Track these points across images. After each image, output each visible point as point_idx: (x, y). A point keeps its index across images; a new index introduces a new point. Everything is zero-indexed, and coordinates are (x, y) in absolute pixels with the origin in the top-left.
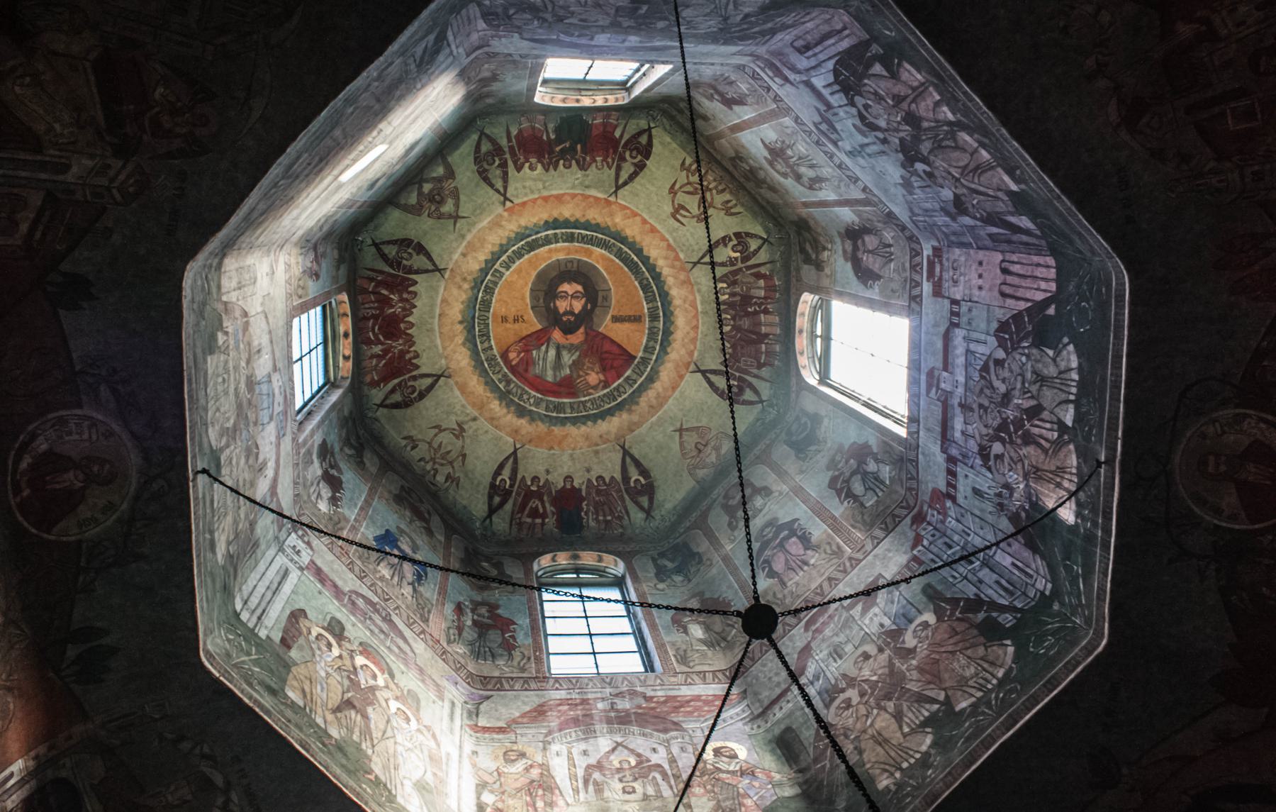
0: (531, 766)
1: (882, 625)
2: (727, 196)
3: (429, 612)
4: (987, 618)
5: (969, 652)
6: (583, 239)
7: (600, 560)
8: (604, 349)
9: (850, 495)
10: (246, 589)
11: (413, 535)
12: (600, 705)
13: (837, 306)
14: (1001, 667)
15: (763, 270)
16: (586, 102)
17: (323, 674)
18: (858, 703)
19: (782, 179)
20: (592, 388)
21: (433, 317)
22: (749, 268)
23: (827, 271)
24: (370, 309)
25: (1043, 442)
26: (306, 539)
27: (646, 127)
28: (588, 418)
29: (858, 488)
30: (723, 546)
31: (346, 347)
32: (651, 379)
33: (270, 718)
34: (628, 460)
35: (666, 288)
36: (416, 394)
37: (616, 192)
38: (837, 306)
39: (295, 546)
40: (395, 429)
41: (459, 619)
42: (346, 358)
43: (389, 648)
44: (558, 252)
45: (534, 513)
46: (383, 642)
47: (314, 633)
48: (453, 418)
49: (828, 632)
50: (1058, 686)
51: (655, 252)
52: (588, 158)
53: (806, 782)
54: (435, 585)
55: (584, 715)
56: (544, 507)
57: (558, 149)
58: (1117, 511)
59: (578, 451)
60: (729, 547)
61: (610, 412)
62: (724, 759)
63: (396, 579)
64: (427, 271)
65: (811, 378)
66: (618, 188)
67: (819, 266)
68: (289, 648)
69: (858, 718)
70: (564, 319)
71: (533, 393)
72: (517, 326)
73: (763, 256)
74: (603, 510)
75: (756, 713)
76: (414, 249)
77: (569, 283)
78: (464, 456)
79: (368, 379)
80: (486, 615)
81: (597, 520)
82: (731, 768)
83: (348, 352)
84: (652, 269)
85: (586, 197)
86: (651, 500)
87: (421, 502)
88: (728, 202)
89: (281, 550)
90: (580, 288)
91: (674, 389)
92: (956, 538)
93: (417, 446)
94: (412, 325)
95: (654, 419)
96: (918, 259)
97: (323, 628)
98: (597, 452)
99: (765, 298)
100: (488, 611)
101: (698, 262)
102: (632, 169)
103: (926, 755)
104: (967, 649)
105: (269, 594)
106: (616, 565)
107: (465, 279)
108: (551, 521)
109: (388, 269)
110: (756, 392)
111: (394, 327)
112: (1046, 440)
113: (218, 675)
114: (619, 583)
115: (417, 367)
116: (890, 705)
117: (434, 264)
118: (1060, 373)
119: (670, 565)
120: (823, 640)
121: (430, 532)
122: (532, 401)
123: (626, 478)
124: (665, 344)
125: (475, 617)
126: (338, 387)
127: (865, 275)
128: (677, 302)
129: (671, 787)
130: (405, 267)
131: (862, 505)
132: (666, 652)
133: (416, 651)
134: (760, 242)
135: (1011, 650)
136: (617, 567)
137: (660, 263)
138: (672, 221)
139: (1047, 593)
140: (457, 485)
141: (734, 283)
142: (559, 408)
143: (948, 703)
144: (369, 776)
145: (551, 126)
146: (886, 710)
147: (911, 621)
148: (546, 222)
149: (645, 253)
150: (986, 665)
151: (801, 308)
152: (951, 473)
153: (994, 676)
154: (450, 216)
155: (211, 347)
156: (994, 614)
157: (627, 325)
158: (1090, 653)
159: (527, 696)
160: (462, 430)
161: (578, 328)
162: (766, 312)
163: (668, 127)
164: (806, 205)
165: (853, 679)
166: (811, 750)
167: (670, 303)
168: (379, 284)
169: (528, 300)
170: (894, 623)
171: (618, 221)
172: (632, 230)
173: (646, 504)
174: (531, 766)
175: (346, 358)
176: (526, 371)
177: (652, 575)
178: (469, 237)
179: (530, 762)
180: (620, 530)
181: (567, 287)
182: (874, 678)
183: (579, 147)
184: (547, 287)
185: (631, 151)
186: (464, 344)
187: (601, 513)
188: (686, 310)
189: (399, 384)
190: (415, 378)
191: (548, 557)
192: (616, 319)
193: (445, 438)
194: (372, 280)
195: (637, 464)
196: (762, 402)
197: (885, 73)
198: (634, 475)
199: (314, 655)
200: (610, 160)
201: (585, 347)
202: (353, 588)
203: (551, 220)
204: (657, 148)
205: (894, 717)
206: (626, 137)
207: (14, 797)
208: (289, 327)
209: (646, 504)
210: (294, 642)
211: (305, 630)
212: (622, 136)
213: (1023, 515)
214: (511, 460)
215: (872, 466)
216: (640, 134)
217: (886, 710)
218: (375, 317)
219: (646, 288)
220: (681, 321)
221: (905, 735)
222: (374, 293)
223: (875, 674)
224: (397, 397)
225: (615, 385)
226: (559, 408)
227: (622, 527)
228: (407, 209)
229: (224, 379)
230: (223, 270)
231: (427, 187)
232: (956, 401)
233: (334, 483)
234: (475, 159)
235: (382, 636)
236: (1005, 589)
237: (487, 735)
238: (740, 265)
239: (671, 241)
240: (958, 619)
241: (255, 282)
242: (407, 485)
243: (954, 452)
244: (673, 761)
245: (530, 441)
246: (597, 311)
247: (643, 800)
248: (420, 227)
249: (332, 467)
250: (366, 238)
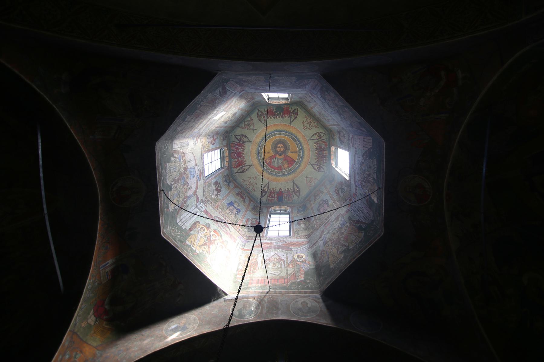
0: (253, 259)
1: (339, 226)
2: (315, 124)
3: (238, 221)
4: (360, 225)
5: (354, 234)
6: (283, 134)
7: (286, 208)
8: (288, 159)
9: (338, 194)
10: (182, 217)
11: (239, 203)
12: (274, 244)
13: (339, 149)
14: (360, 238)
15: (324, 141)
16: (281, 103)
17: (200, 237)
18: (331, 245)
19: (322, 119)
20: (286, 168)
21: (249, 152)
22: (321, 140)
23: (335, 141)
24: (233, 150)
25: (371, 182)
26: (205, 204)
27: (296, 108)
28: (285, 175)
29: (340, 192)
30: (312, 205)
31: (227, 159)
32: (299, 166)
33: (178, 248)
34: (294, 185)
35: (302, 145)
36: (245, 170)
37: (290, 123)
38: (339, 149)
39: (201, 206)
40: (240, 178)
41: (247, 222)
42: (227, 162)
43: (223, 230)
44: (278, 137)
45: (272, 197)
46: (221, 229)
47: (200, 227)
48: (254, 175)
49: (328, 227)
50: (371, 244)
51: (300, 137)
52: (284, 116)
53: (317, 265)
54: (242, 214)
55: (270, 246)
56: (275, 195)
57: (276, 114)
58: (384, 201)
59: (283, 183)
60: (313, 205)
61: (290, 174)
62: (300, 258)
63: (230, 213)
64: (247, 142)
65: (334, 166)
66: (291, 122)
67: (334, 140)
68: (191, 231)
69: (330, 249)
70: (279, 152)
71: (272, 169)
72: (268, 154)
73: (324, 138)
74: (288, 196)
75: (311, 246)
76: (244, 137)
77: (280, 144)
78: (256, 184)
79: (233, 166)
80: (255, 221)
81: (287, 198)
82: (300, 261)
83: (227, 160)
84: (299, 141)
85: (283, 125)
86: (299, 194)
87: (244, 195)
88: (316, 125)
89: (197, 207)
90: (282, 145)
91: (305, 168)
92: (357, 205)
93: (245, 182)
94: (244, 154)
95: (300, 175)
96: (349, 138)
97: (204, 226)
98: (287, 183)
99: (325, 147)
100: (256, 220)
101: (310, 139)
102: (294, 118)
103: (342, 260)
104: (354, 233)
105: (190, 218)
106: (289, 209)
107: (256, 144)
108: (276, 199)
109: (238, 141)
110: (323, 169)
111: (239, 155)
112: (371, 182)
113: (165, 238)
114: (289, 214)
115: (246, 164)
116: (337, 246)
117: (249, 140)
118: (374, 166)
119: (301, 209)
120: (327, 229)
121: (244, 202)
122: (272, 171)
123: (294, 189)
124: (302, 158)
125: (252, 222)
126: (224, 168)
127: (342, 142)
128: (305, 148)
129: (285, 265)
130: (242, 141)
131: (340, 196)
132: (294, 231)
133: (231, 230)
134: (324, 134)
135: (363, 234)
136: (289, 210)
137: (301, 139)
138: (303, 129)
139: (373, 220)
140: (254, 191)
141: (318, 144)
142: (278, 173)
143: (348, 247)
144: (205, 262)
145: (274, 108)
146: (335, 247)
147: (344, 225)
148: (275, 130)
149: (297, 137)
150: (357, 238)
151: (332, 149)
152: (356, 189)
153: (359, 240)
154: (252, 129)
155: (169, 160)
156: (361, 225)
157: (293, 154)
158: (379, 236)
159: (258, 241)
160: (256, 178)
161: (282, 154)
162: (325, 150)
163: (301, 108)
164: (329, 125)
165: (331, 239)
166: (319, 257)
167: (303, 148)
168: (236, 145)
169: (271, 148)
170: (341, 226)
171: (291, 130)
172: (294, 132)
173: (298, 195)
174: (253, 259)
175: (227, 162)
176: (271, 164)
177: (296, 212)
178: (257, 134)
179: (253, 258)
180: (292, 201)
181: (279, 145)
182: (335, 239)
183: (281, 113)
184: (275, 145)
185: (293, 114)
186: (256, 158)
187: (288, 197)
188: (307, 150)
189: (241, 168)
190: (245, 166)
191: (274, 207)
192: (291, 152)
193: (252, 180)
194: (234, 144)
195: (296, 185)
196: (324, 171)
197: (328, 94)
198: (296, 188)
199: (198, 232)
200: (289, 116)
201: (284, 159)
202: (216, 216)
203: (276, 130)
204: (299, 113)
205: (337, 249)
206: (292, 111)
207: (109, 268)
208: (202, 156)
209: (298, 195)
210: (193, 229)
211: (198, 226)
212: (291, 110)
213: (368, 200)
214: (267, 185)
215: (343, 187)
216: (295, 110)
217: (335, 247)
218: (235, 152)
219: (298, 145)
220: (306, 153)
221: (338, 254)
222: (235, 147)
223: (335, 238)
224: (241, 171)
225: (291, 167)
226: (278, 173)
227: (292, 200)
228: (241, 128)
229: (174, 169)
230: (173, 143)
231: (246, 123)
232: (356, 172)
233: (218, 191)
234: (258, 116)
235: (221, 227)
236: (365, 218)
237: (245, 251)
238: (319, 140)
239: (303, 134)
240: (354, 225)
241: (188, 146)
242: (241, 191)
243: (356, 184)
244: (287, 258)
245: (272, 180)
246: (287, 150)
247: (277, 268)
248: (245, 132)
249: (219, 187)
250: (232, 134)
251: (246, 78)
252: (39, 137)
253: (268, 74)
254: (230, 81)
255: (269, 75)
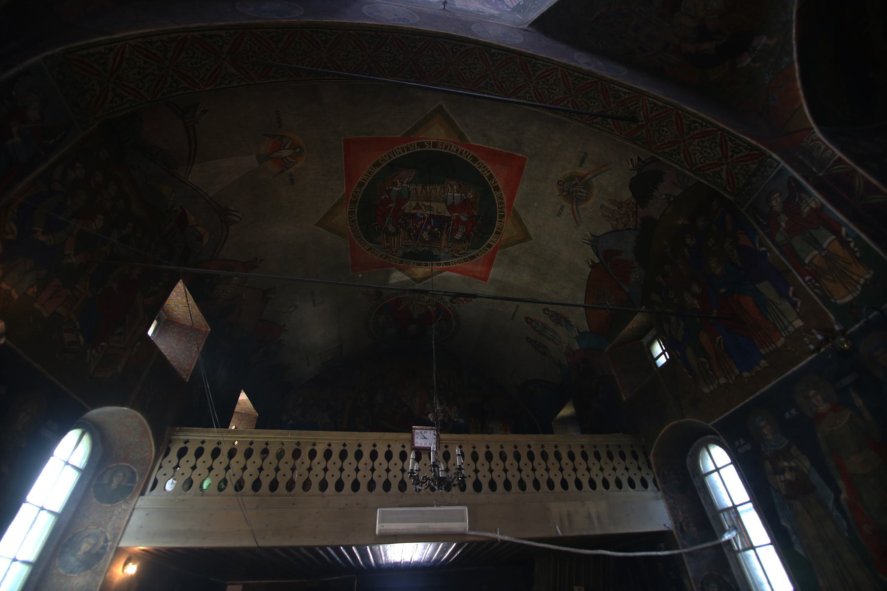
42: (497, 188)
251: (485, 8)
252: (340, 562)
253: (447, 11)
254: (512, 7)
255: (446, 8)
